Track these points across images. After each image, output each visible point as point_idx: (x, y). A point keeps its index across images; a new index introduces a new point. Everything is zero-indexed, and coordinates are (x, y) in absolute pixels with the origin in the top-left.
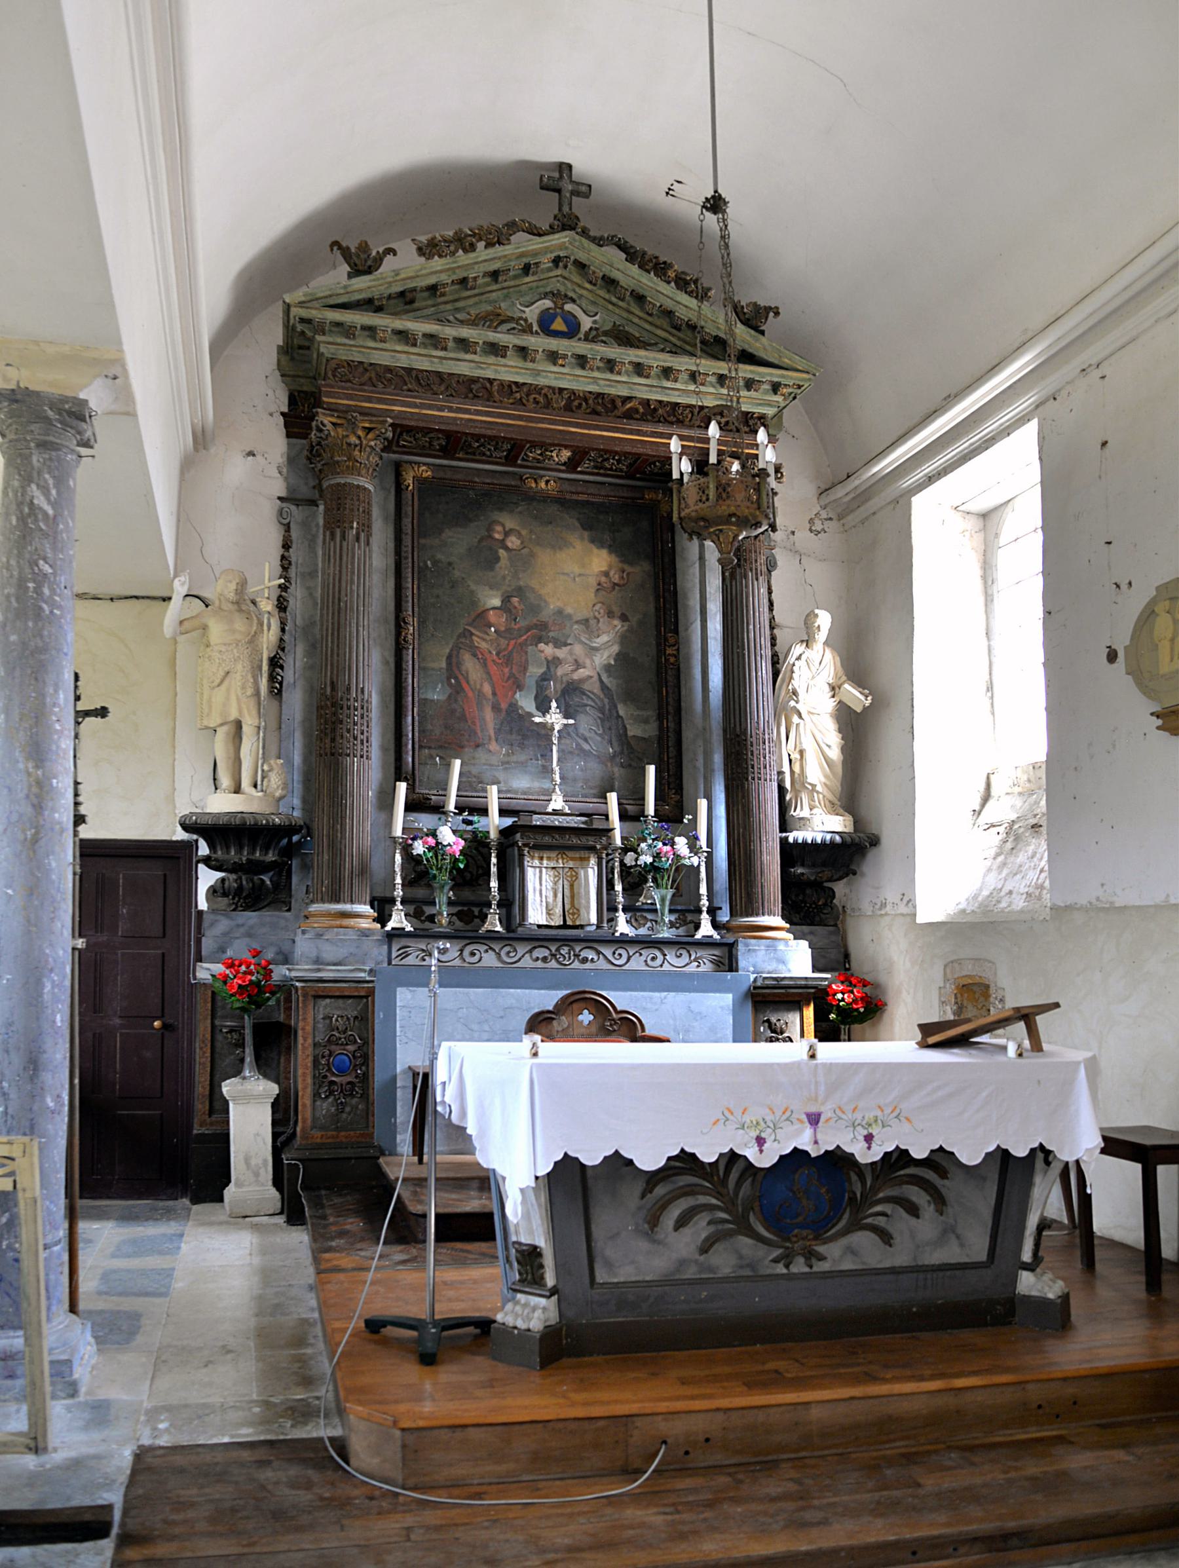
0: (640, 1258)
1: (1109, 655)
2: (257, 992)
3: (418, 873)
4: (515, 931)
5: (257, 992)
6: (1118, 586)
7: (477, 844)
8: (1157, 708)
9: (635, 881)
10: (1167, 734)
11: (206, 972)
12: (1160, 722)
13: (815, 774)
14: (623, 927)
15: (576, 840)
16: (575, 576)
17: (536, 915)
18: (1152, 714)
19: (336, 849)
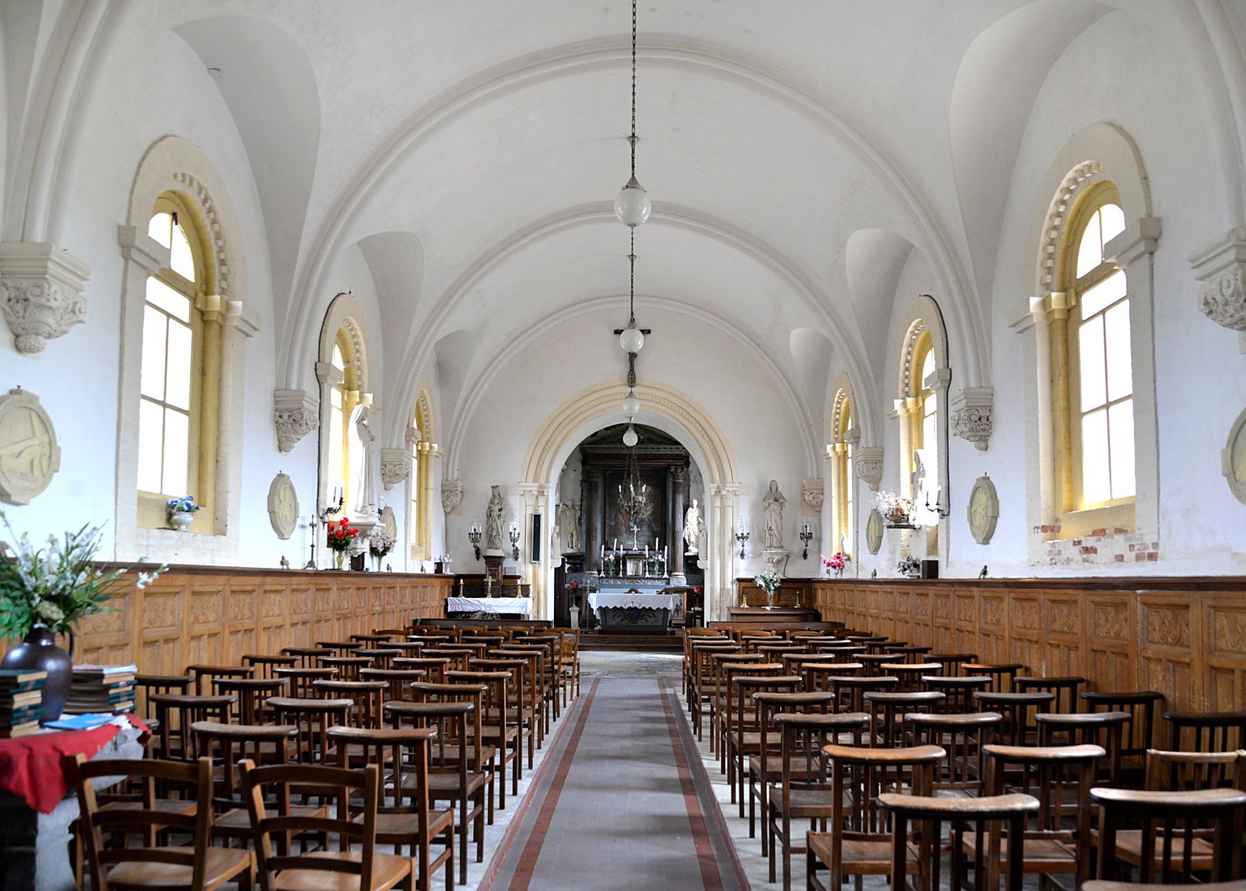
0: (613, 622)
2: (575, 590)
3: (606, 565)
4: (625, 577)
5: (575, 590)
7: (617, 558)
9: (652, 565)
11: (567, 586)
13: (693, 539)
14: (647, 575)
15: (638, 557)
16: (641, 494)
17: (629, 573)
19: (590, 559)
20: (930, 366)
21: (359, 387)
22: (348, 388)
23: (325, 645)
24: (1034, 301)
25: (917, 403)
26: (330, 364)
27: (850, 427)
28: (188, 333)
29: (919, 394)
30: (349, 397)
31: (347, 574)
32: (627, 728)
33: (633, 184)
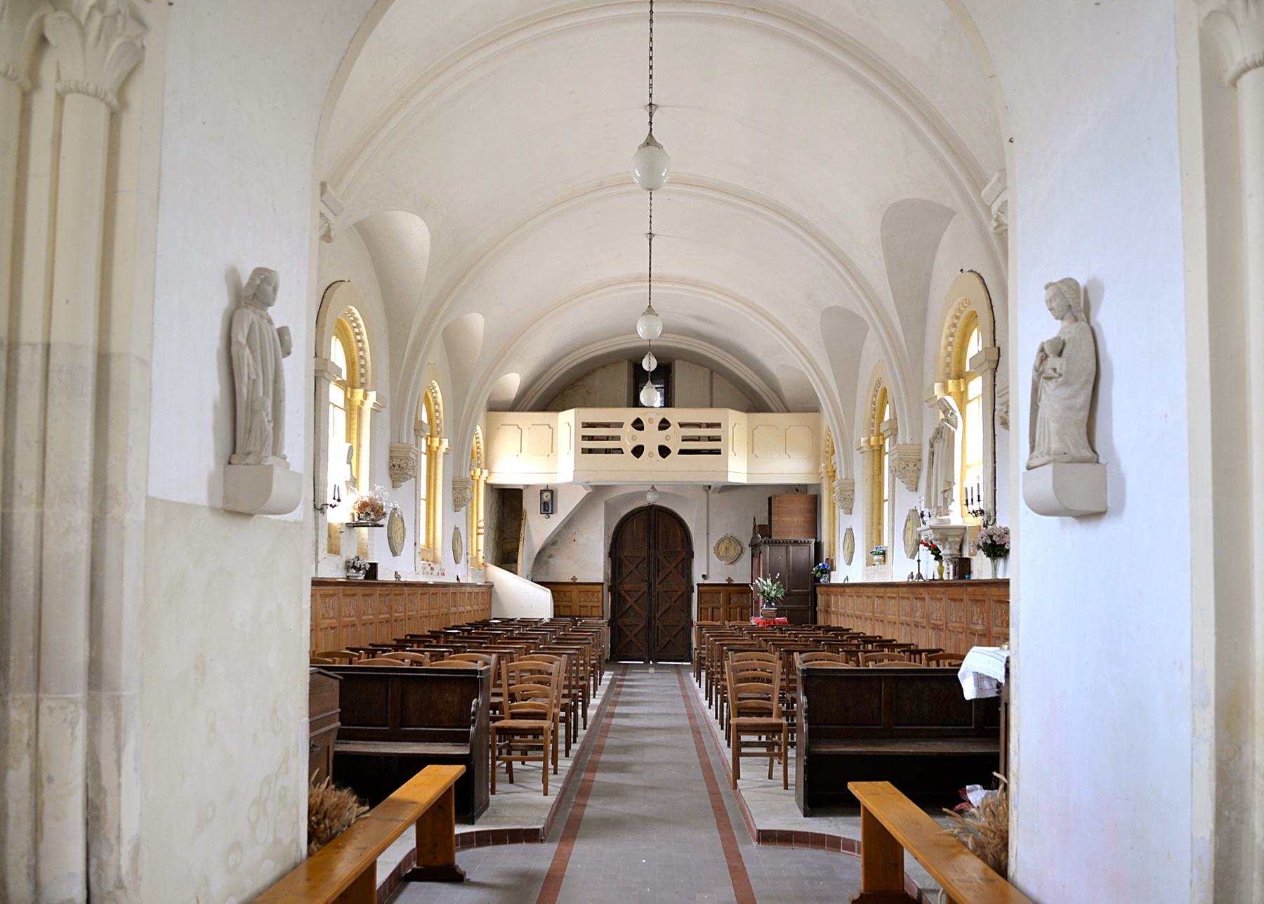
20: (975, 346)
21: (362, 385)
22: (350, 385)
23: (412, 636)
24: (863, 439)
25: (958, 386)
26: (327, 360)
27: (887, 417)
28: (343, 413)
29: (961, 376)
30: (352, 393)
31: (947, 585)
32: (649, 756)
33: (650, 141)
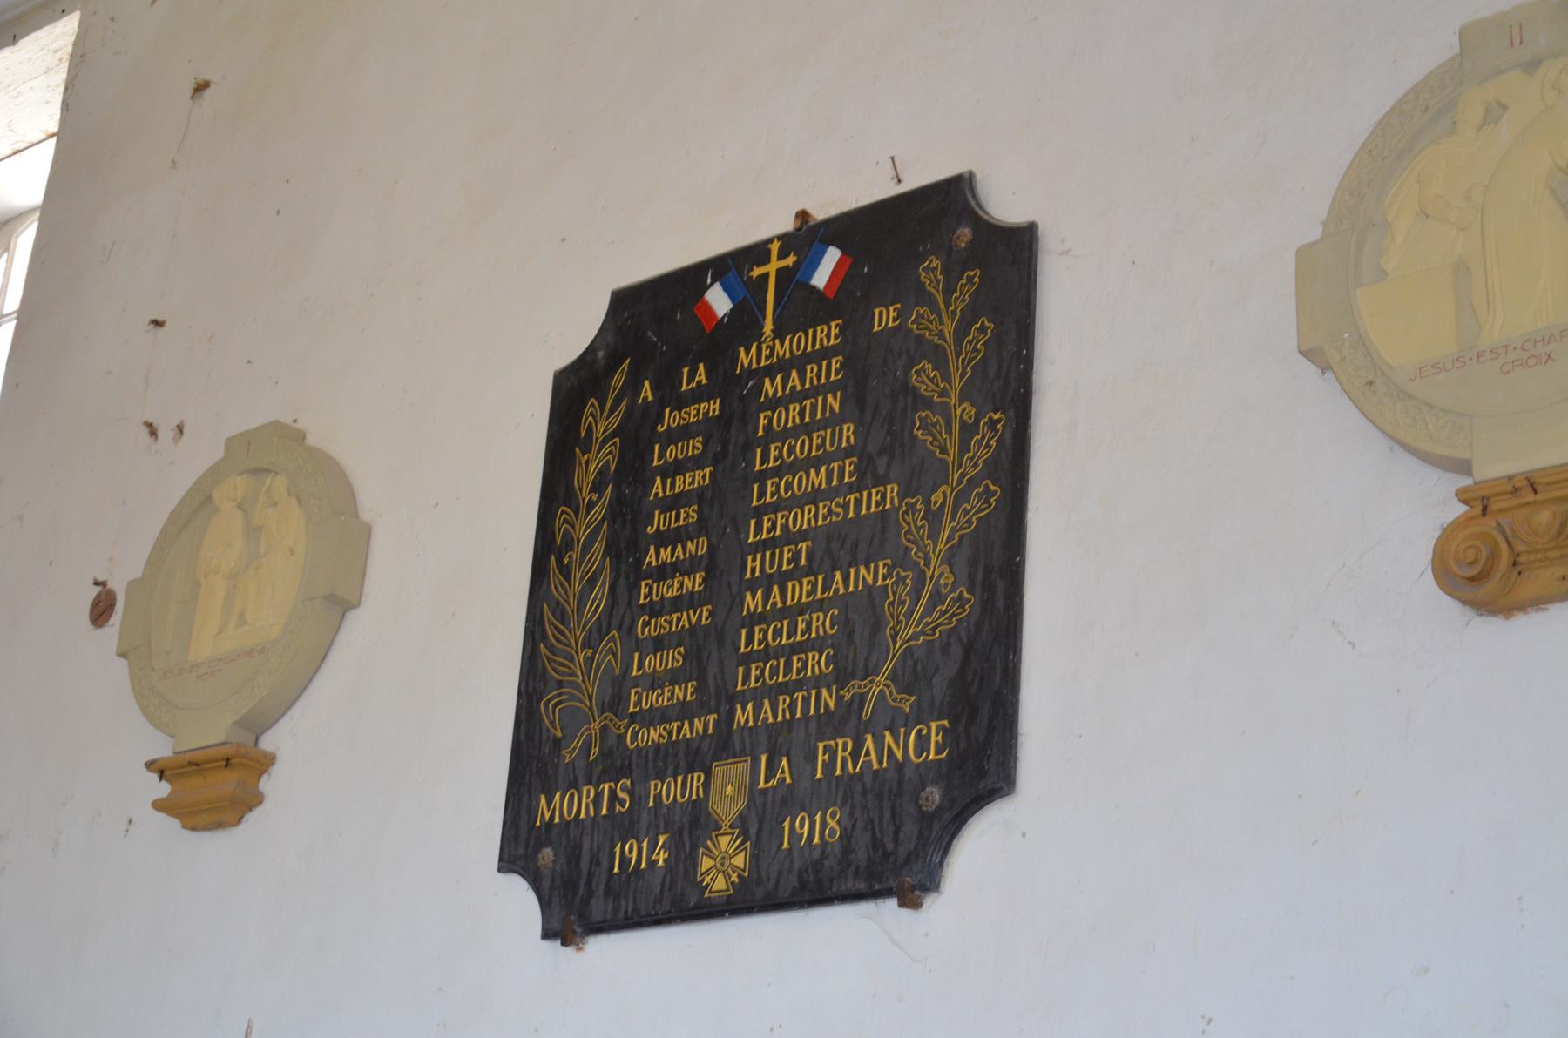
1: (96, 603)
6: (153, 433)
8: (163, 749)
10: (174, 823)
12: (163, 789)
18: (150, 765)
